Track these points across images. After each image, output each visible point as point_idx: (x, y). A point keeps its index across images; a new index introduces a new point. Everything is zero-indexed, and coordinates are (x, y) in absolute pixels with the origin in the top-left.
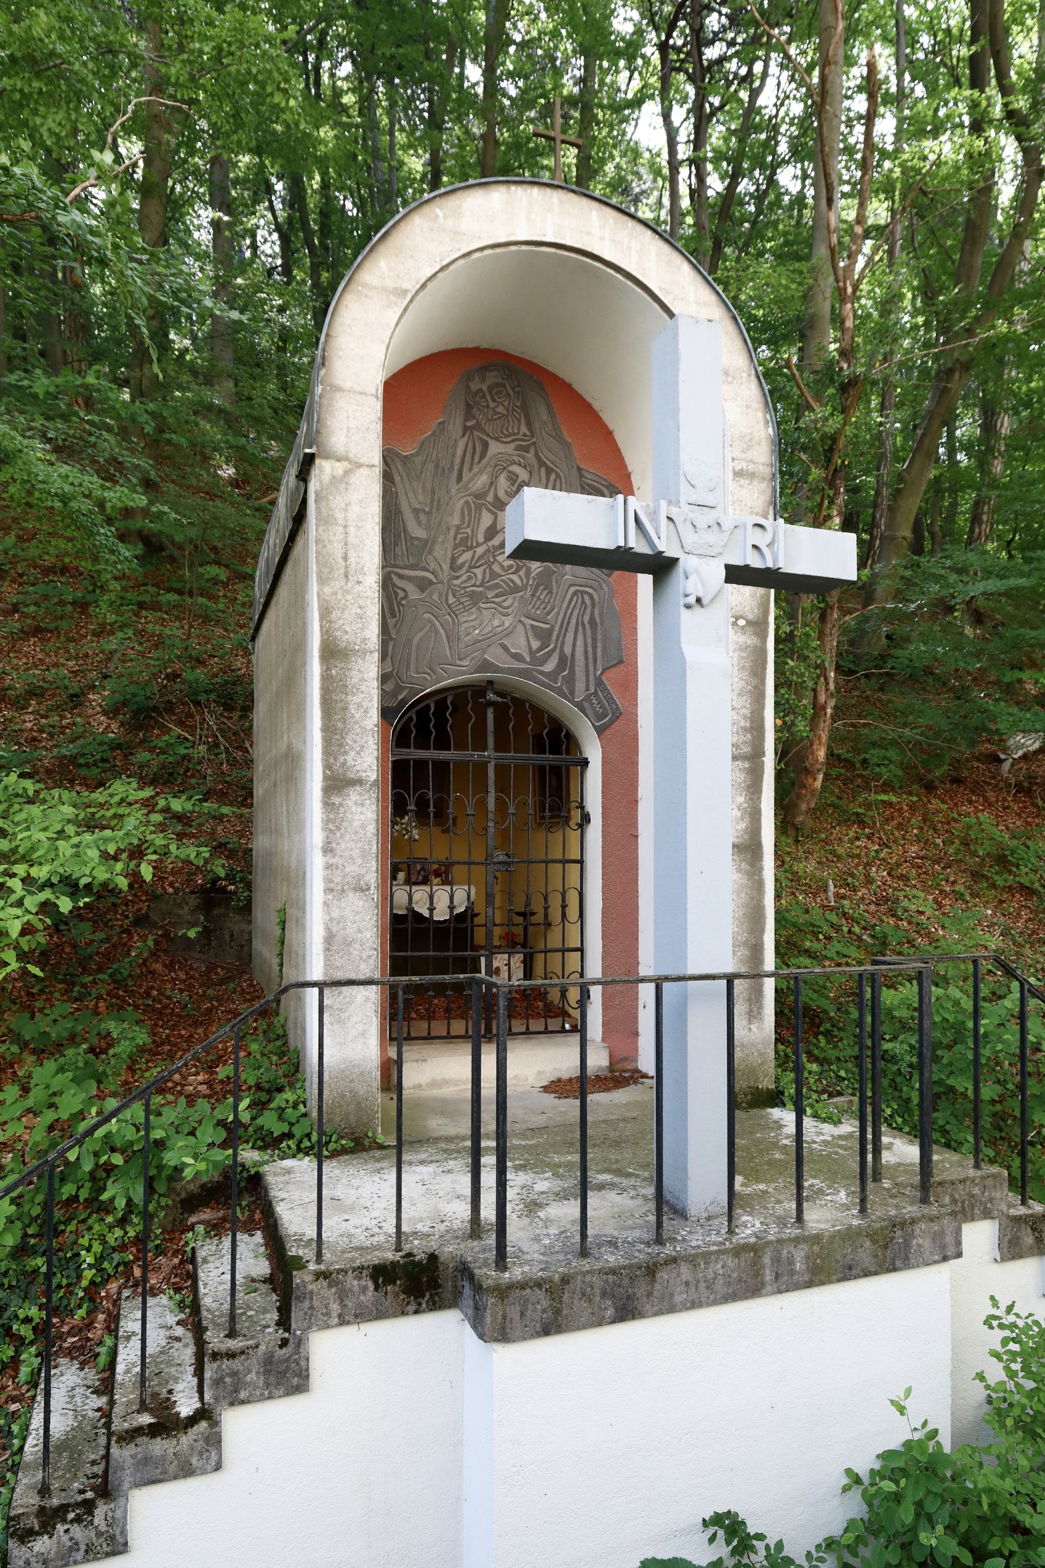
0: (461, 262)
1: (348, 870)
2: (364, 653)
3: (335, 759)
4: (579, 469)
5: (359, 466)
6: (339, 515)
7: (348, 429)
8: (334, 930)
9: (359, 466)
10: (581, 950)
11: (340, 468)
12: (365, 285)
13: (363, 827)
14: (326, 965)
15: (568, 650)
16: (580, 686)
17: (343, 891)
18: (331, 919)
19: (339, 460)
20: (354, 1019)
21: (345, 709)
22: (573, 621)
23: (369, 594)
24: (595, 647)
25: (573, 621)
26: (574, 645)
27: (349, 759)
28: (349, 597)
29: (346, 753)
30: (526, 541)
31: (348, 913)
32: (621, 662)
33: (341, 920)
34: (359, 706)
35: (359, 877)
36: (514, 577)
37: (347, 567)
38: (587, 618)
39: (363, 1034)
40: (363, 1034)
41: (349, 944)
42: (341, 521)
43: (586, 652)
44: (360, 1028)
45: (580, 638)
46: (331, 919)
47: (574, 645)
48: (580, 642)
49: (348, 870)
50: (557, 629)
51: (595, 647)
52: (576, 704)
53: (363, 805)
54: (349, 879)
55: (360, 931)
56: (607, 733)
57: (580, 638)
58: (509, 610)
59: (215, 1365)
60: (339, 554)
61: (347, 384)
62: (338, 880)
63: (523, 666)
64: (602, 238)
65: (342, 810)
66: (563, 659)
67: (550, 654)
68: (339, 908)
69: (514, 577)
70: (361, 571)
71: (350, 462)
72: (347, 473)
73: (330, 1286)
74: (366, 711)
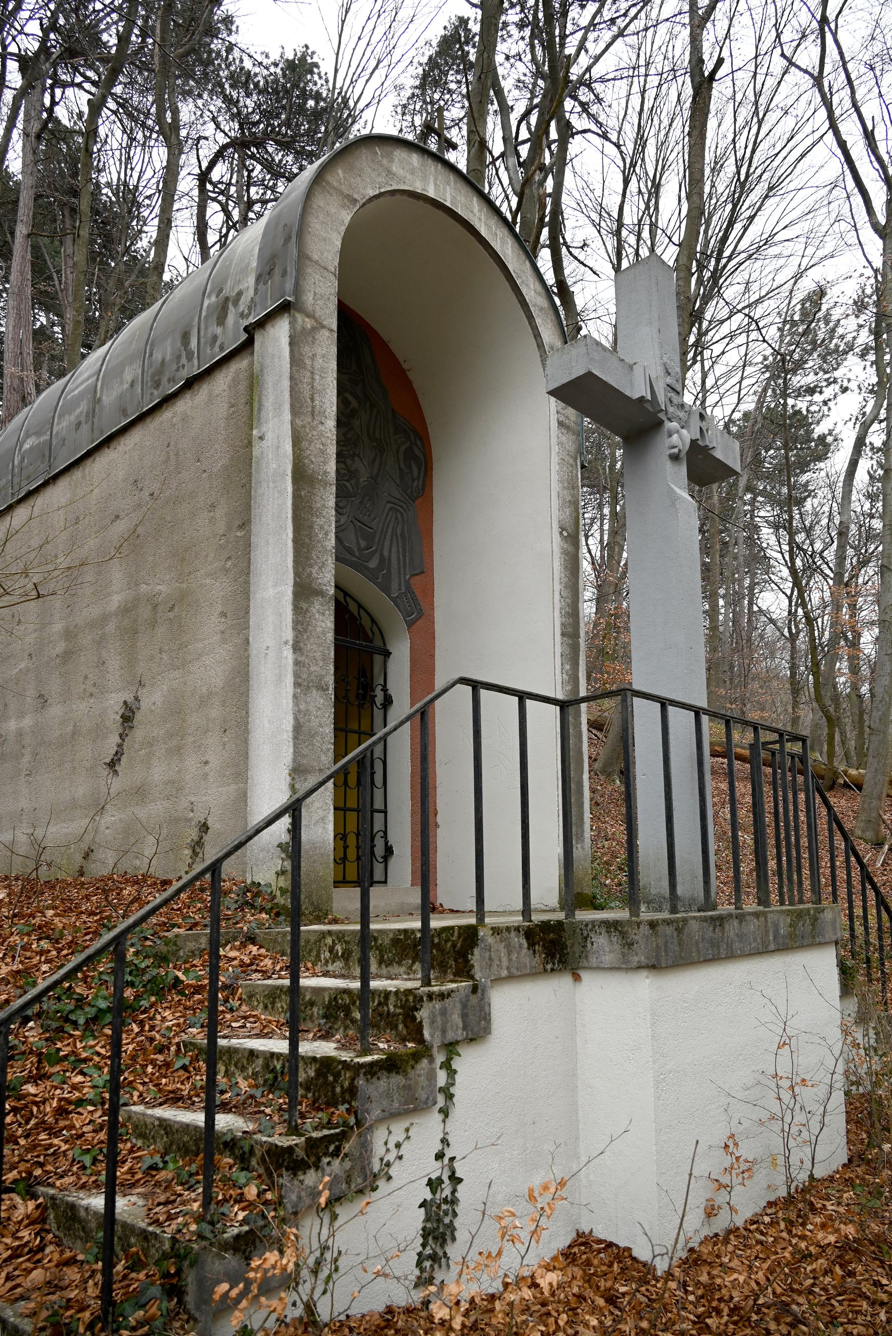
0: (388, 198)
1: (312, 669)
2: (326, 484)
3: (303, 569)
4: (393, 410)
5: (323, 327)
6: (308, 362)
7: (315, 294)
8: (302, 721)
9: (323, 327)
10: (385, 812)
11: (309, 323)
12: (328, 183)
13: (324, 633)
14: (295, 752)
15: (386, 554)
16: (394, 586)
17: (308, 687)
18: (299, 711)
19: (308, 316)
20: (316, 804)
21: (311, 527)
22: (390, 531)
23: (329, 435)
24: (404, 556)
25: (390, 531)
26: (390, 551)
27: (314, 570)
28: (315, 433)
29: (311, 566)
30: (589, 375)
31: (312, 708)
32: (423, 572)
33: (307, 713)
34: (322, 527)
35: (321, 677)
36: (348, 484)
37: (313, 407)
38: (399, 532)
39: (323, 819)
40: (323, 819)
41: (313, 736)
42: (309, 367)
43: (399, 558)
44: (321, 813)
45: (394, 546)
46: (299, 711)
47: (390, 551)
48: (394, 550)
49: (312, 669)
50: (378, 534)
51: (404, 556)
52: (392, 599)
53: (323, 614)
54: (313, 677)
55: (321, 726)
56: (415, 627)
57: (394, 546)
58: (344, 511)
59: (431, 1005)
60: (307, 394)
61: (315, 257)
62: (305, 676)
63: (354, 559)
64: (480, 219)
65: (308, 615)
66: (382, 560)
67: (373, 554)
68: (306, 702)
69: (348, 484)
70: (323, 413)
71: (316, 321)
72: (314, 329)
73: (501, 941)
74: (326, 534)
